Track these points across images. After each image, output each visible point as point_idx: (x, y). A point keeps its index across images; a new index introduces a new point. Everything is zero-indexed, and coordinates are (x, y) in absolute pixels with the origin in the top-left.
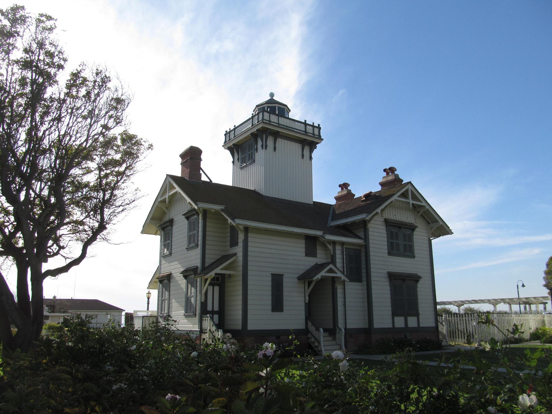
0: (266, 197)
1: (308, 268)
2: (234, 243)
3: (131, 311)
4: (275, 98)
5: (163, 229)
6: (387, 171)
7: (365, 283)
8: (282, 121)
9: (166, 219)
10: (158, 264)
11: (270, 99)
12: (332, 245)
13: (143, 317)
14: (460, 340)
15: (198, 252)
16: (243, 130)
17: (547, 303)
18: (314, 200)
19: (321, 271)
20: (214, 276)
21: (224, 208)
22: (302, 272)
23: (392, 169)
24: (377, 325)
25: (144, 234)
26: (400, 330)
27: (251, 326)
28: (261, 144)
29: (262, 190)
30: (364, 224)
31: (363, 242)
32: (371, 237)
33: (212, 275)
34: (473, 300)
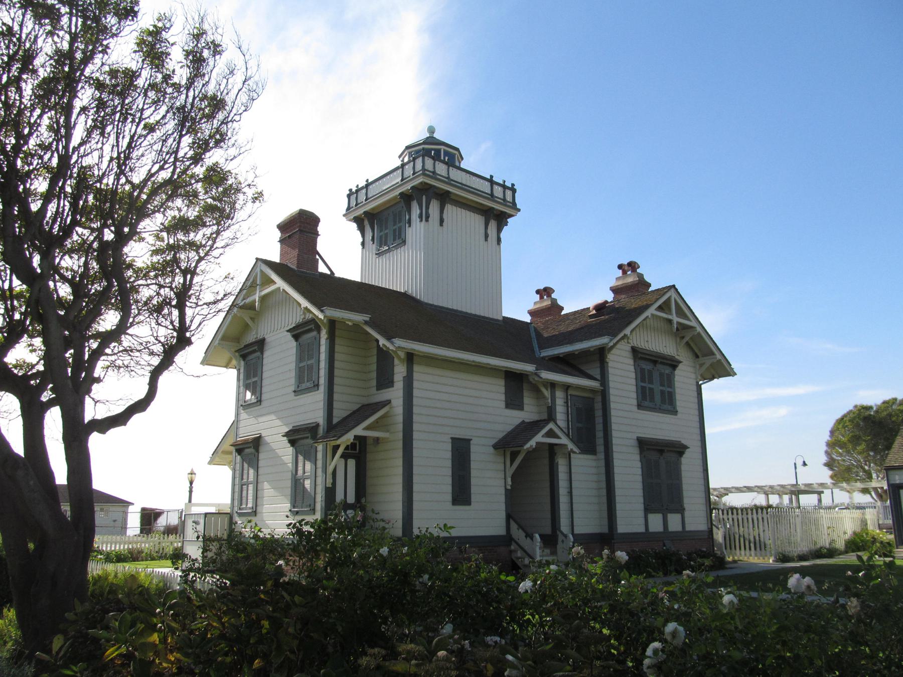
0: (427, 304)
1: (509, 428)
2: (385, 381)
3: (153, 504)
4: (435, 135)
5: (244, 357)
6: (623, 267)
7: (602, 456)
9: (251, 338)
10: (232, 418)
13: (206, 514)
14: (743, 552)
15: (319, 396)
16: (384, 188)
17: (823, 492)
18: (504, 315)
19: (536, 434)
20: (352, 441)
22: (501, 435)
23: (633, 265)
25: (206, 366)
28: (418, 212)
29: (420, 292)
30: (601, 354)
31: (599, 385)
32: (611, 378)
33: (350, 439)
34: (745, 487)
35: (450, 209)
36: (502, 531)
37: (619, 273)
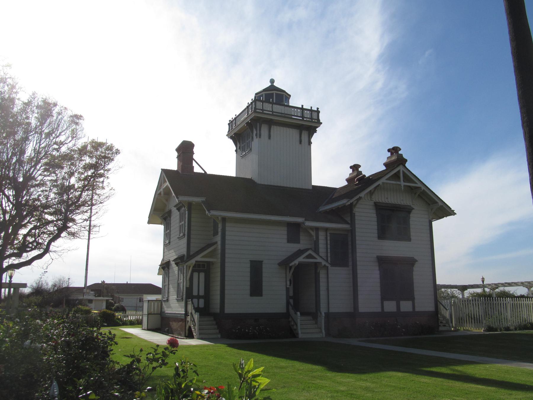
4: (275, 84)
6: (391, 151)
7: (351, 267)
8: (278, 108)
9: (167, 210)
11: (271, 85)
12: (314, 231)
20: (194, 264)
21: (205, 200)
24: (363, 308)
25: (150, 224)
26: (390, 314)
27: (228, 310)
28: (256, 132)
30: (351, 208)
35: (275, 130)
36: (284, 311)
37: (389, 154)
